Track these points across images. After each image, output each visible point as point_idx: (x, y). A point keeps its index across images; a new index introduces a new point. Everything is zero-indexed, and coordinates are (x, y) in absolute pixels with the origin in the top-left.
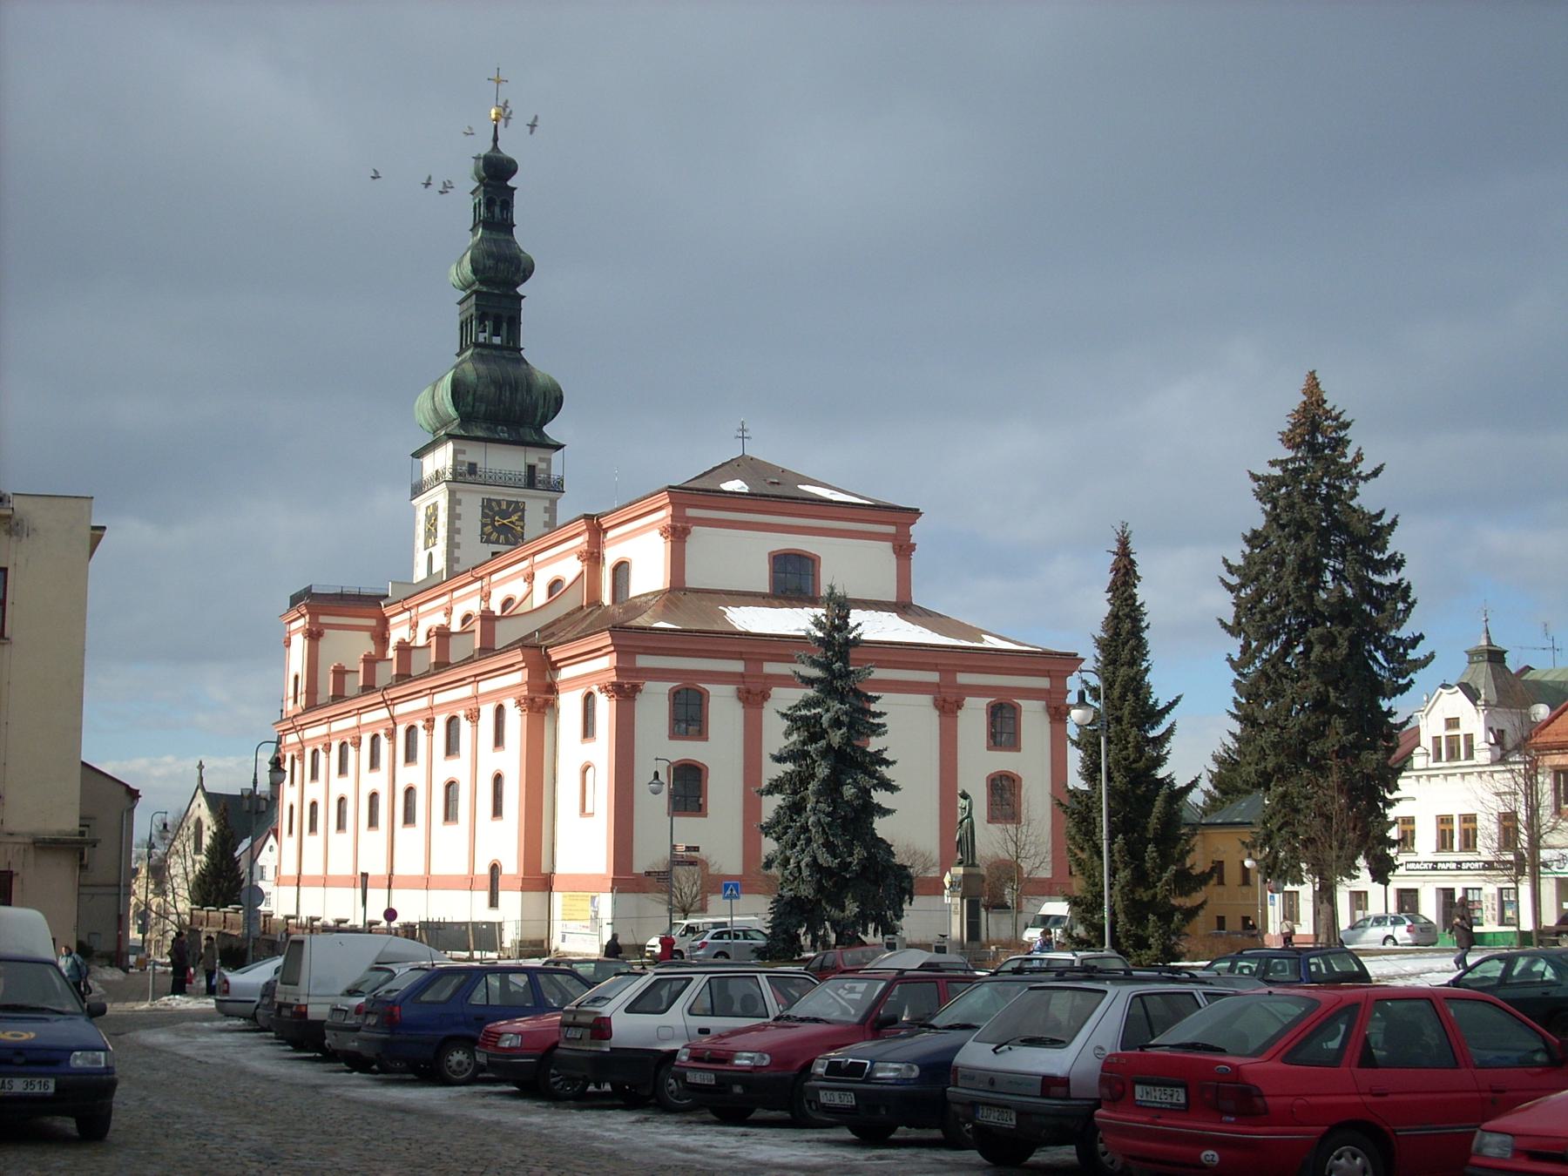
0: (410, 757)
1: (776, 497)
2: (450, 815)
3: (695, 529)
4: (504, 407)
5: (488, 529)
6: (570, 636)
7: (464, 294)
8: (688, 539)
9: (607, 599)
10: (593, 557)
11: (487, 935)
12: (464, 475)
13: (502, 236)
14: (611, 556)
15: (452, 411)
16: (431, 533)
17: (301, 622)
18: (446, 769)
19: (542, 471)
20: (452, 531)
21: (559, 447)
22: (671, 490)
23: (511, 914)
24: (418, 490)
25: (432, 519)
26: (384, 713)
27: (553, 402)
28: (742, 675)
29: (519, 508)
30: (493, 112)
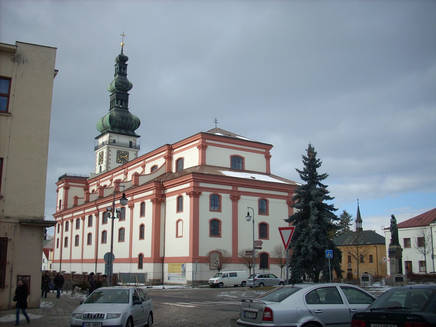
0: (67, 230)
1: (229, 139)
2: (77, 244)
3: (242, 197)
4: (123, 124)
5: (119, 159)
6: (168, 179)
7: (112, 93)
8: (207, 149)
9: (174, 171)
10: (169, 158)
11: (141, 278)
12: (112, 143)
13: (124, 77)
14: (175, 157)
15: (109, 125)
16: (101, 160)
17: (63, 184)
18: (76, 232)
19: (134, 143)
20: (108, 159)
22: (202, 133)
23: (149, 269)
24: (96, 148)
25: (101, 156)
26: (95, 208)
27: (138, 124)
28: (232, 191)
29: (127, 153)
30: (122, 43)
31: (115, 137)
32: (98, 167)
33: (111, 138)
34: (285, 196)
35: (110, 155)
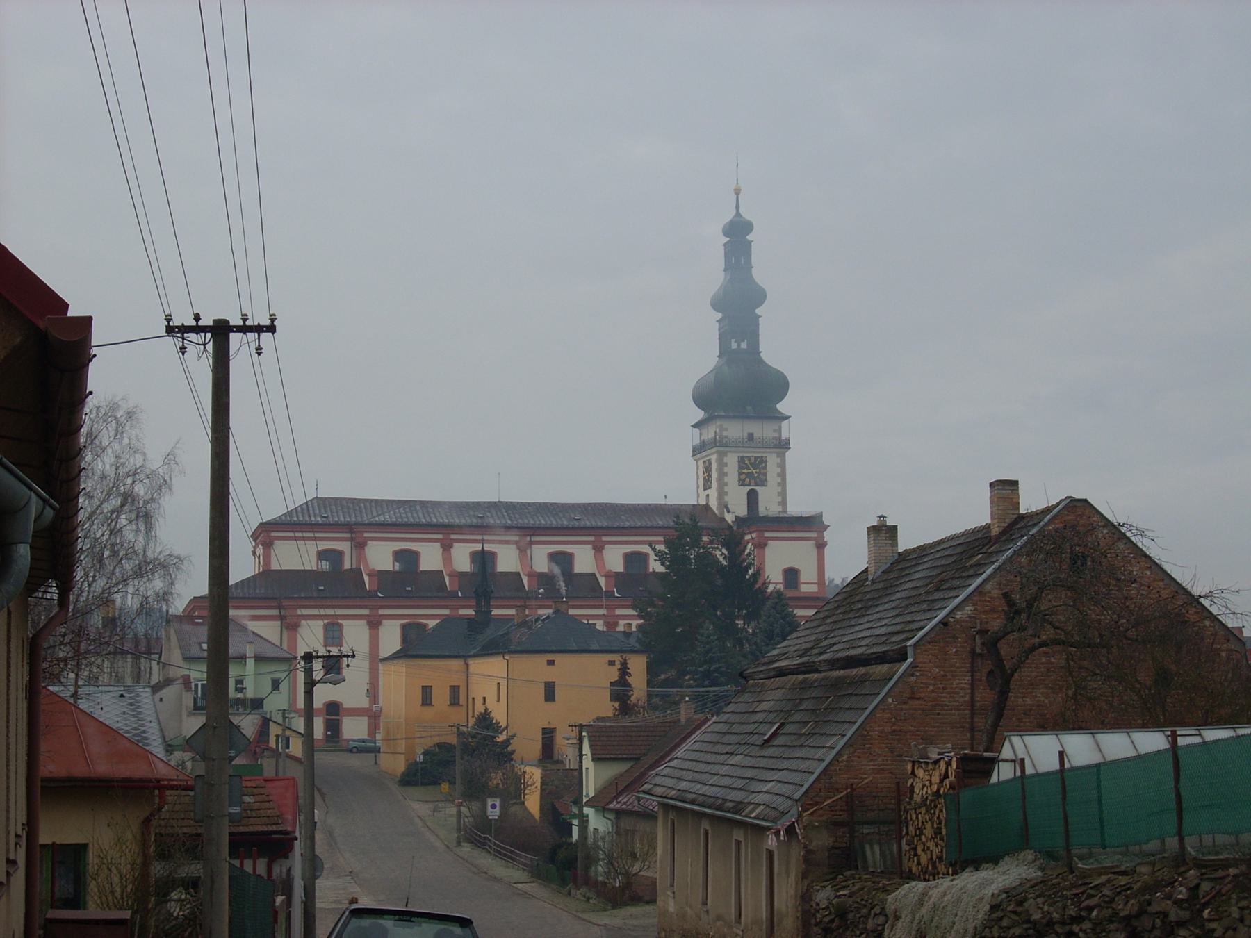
3: (456, 545)
27: (780, 386)
29: (763, 461)
34: (295, 701)
35: (779, 475)
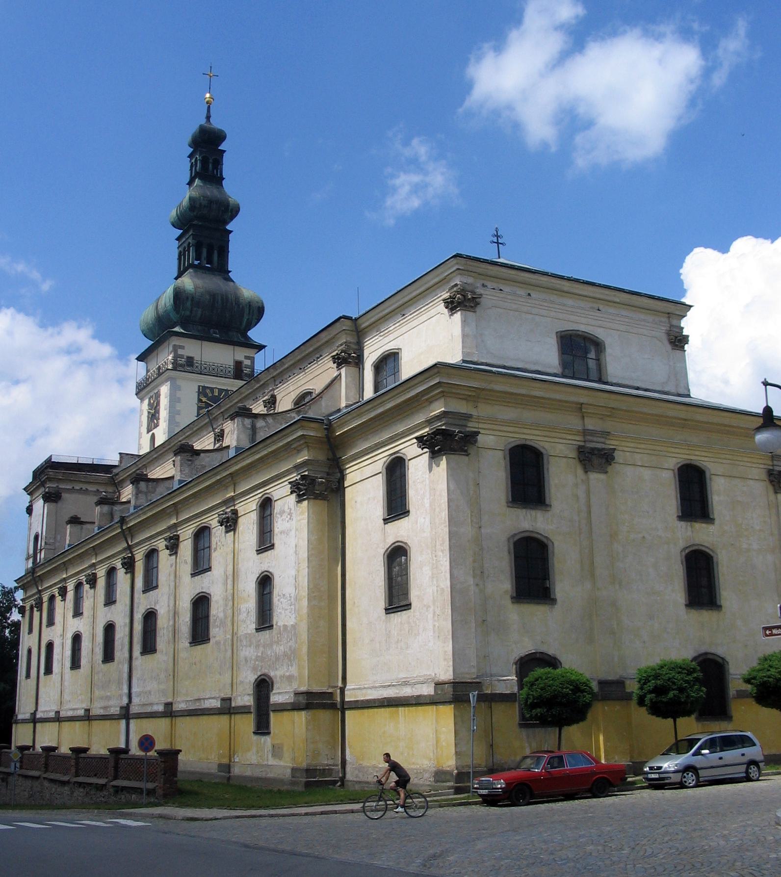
0: (51, 623)
14: (373, 350)
19: (247, 366)
21: (261, 347)
27: (257, 312)
31: (192, 348)
32: (147, 438)
33: (180, 352)
35: (179, 400)
